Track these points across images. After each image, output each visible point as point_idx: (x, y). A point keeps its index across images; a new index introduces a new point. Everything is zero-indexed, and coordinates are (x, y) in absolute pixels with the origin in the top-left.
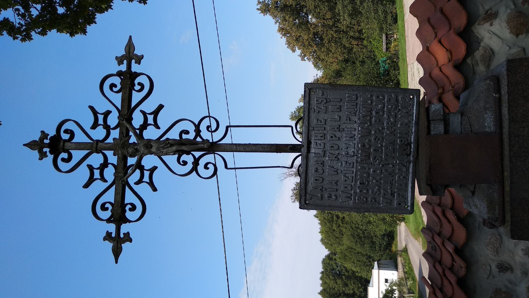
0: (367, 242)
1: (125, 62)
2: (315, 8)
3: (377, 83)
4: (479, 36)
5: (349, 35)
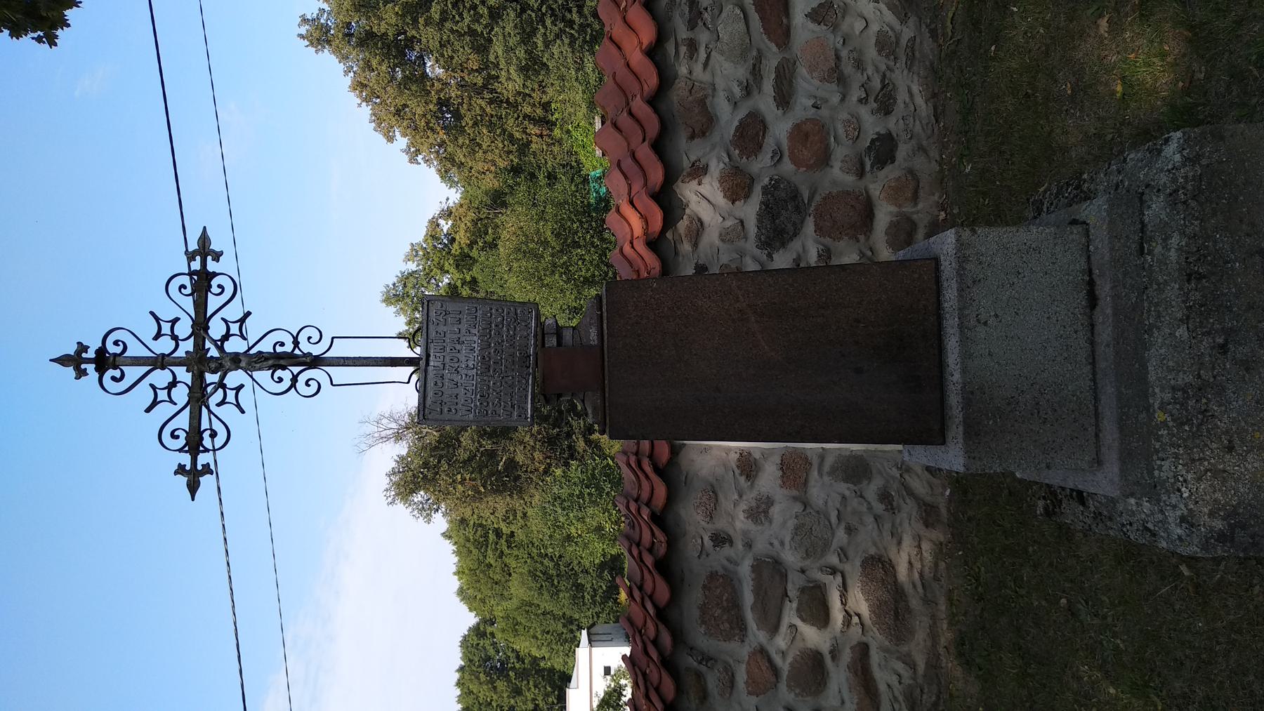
0: (564, 585)
1: (198, 258)
2: (441, 46)
3: (582, 226)
4: (684, 200)
5: (521, 111)
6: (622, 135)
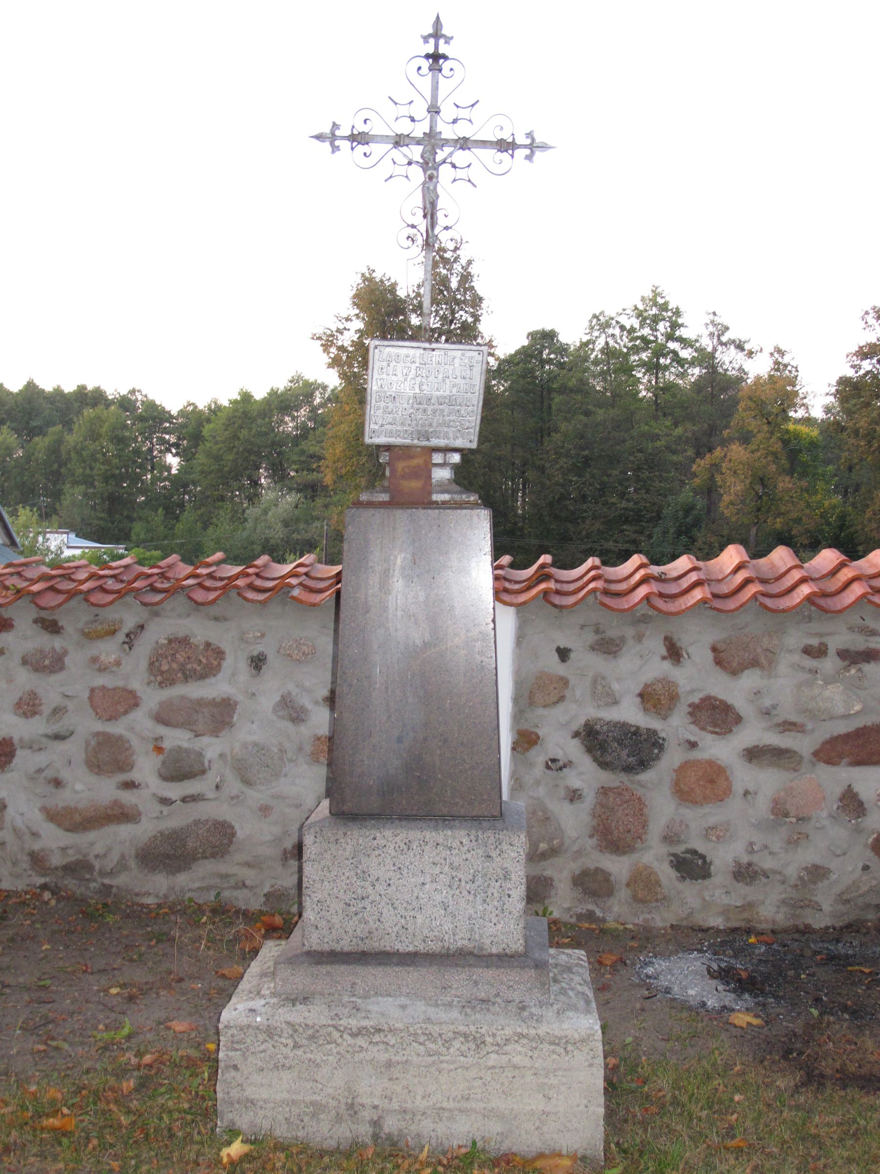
6: (730, 574)
